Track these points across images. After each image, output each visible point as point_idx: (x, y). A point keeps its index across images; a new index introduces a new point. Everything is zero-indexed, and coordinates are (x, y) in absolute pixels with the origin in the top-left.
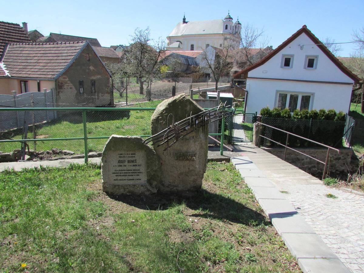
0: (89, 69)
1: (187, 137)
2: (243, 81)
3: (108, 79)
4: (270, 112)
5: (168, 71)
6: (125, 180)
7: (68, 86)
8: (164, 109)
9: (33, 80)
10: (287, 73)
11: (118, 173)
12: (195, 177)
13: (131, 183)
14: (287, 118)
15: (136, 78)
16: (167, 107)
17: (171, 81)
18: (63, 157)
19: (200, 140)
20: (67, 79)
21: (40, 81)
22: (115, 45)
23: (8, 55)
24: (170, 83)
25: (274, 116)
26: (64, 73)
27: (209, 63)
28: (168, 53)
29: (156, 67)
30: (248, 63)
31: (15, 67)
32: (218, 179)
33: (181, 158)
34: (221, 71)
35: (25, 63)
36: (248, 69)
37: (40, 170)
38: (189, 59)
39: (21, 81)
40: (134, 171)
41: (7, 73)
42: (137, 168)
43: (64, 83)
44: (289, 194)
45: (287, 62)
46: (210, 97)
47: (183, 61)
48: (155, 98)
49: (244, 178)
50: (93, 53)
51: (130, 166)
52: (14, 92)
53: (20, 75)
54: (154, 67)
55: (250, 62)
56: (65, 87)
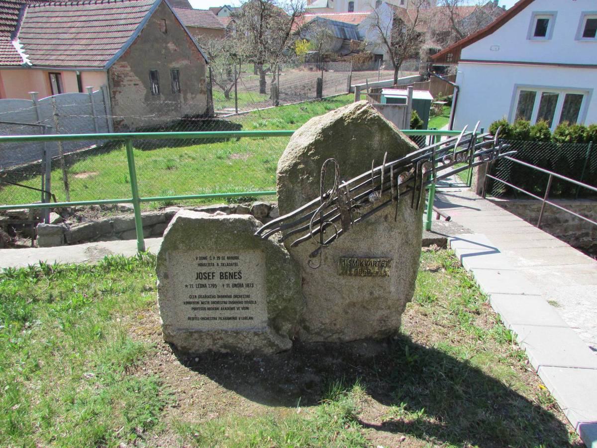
0: (166, 48)
1: (372, 218)
2: (444, 68)
3: (203, 67)
4: (509, 130)
5: (310, 50)
6: (215, 319)
7: (131, 81)
8: (311, 144)
9: (68, 70)
10: (541, 49)
11: (198, 303)
12: (386, 312)
13: (230, 326)
14: (541, 140)
15: (253, 65)
16: (319, 140)
17: (315, 68)
18: (118, 217)
19: (403, 224)
20: (129, 69)
21: (80, 73)
22: (217, 6)
23: (27, 25)
24: (313, 73)
25: (515, 136)
26: (121, 57)
27: (383, 34)
28: (309, 17)
29: (289, 43)
30: (454, 34)
31: (39, 47)
32: (429, 298)
33: (353, 270)
34: (405, 48)
35: (55, 40)
36: (462, 44)
37: (40, 271)
38: (345, 29)
39: (50, 73)
40: (236, 299)
41: (26, 60)
42: (244, 291)
43: (123, 76)
44: (562, 308)
45: (541, 29)
46: (389, 100)
47: (335, 32)
48: (285, 100)
49: (490, 296)
50: (174, 18)
51: (225, 287)
52: (32, 94)
53: (47, 63)
54: (284, 42)
55: (458, 32)
56: (124, 84)
